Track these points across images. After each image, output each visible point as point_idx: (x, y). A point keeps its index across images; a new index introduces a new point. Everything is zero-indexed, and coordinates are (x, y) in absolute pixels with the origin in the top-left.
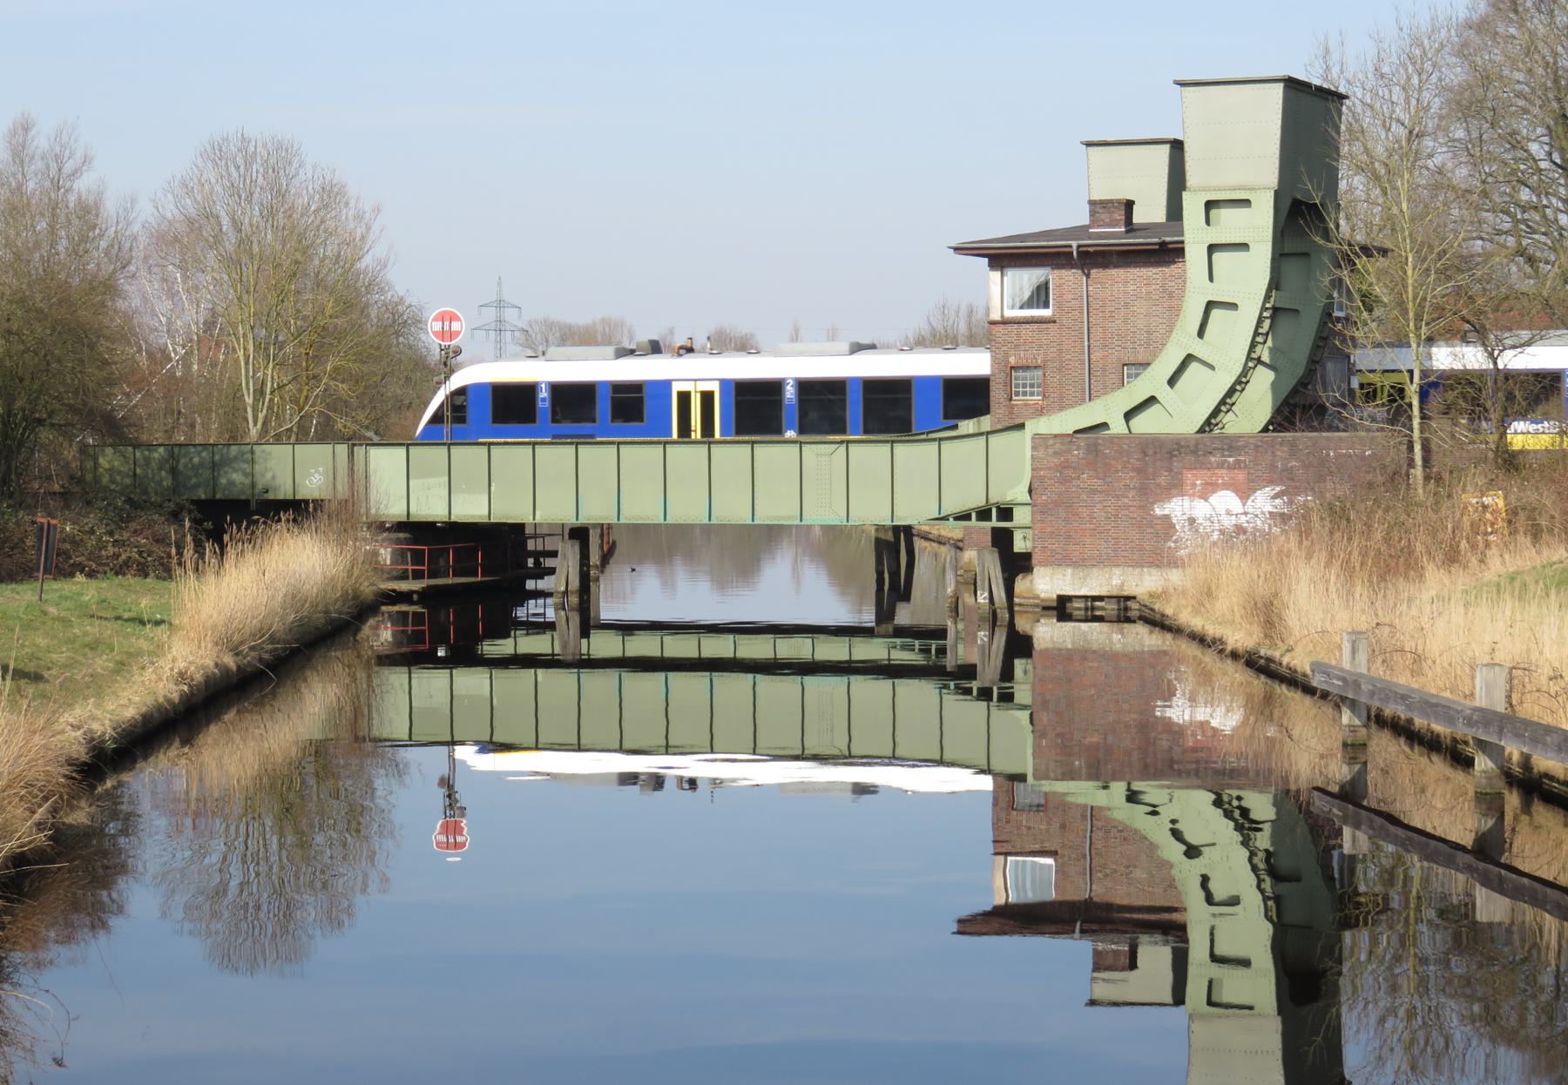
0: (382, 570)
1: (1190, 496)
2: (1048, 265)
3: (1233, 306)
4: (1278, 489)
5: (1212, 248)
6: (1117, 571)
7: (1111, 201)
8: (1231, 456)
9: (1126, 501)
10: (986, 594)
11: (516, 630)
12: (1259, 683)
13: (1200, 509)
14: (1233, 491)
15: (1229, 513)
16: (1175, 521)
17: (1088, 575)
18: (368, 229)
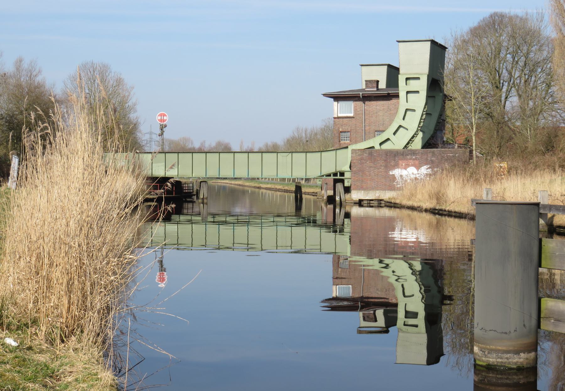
1: (401, 168)
2: (352, 100)
3: (414, 110)
4: (428, 166)
5: (408, 92)
6: (378, 192)
7: (372, 81)
8: (414, 156)
9: (381, 170)
10: (339, 197)
11: (184, 190)
12: (433, 218)
13: (404, 172)
14: (415, 167)
15: (413, 174)
16: (396, 176)
17: (369, 193)
18: (130, 93)
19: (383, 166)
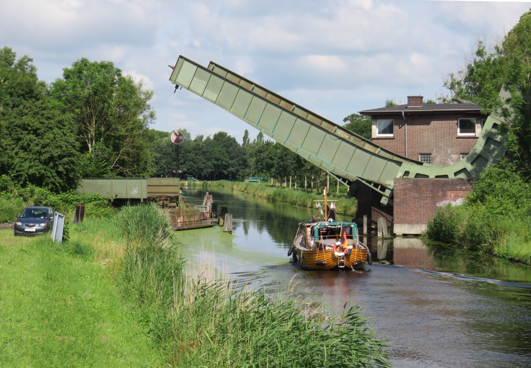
0: (248, 175)
10: (381, 233)
19: (430, 197)
